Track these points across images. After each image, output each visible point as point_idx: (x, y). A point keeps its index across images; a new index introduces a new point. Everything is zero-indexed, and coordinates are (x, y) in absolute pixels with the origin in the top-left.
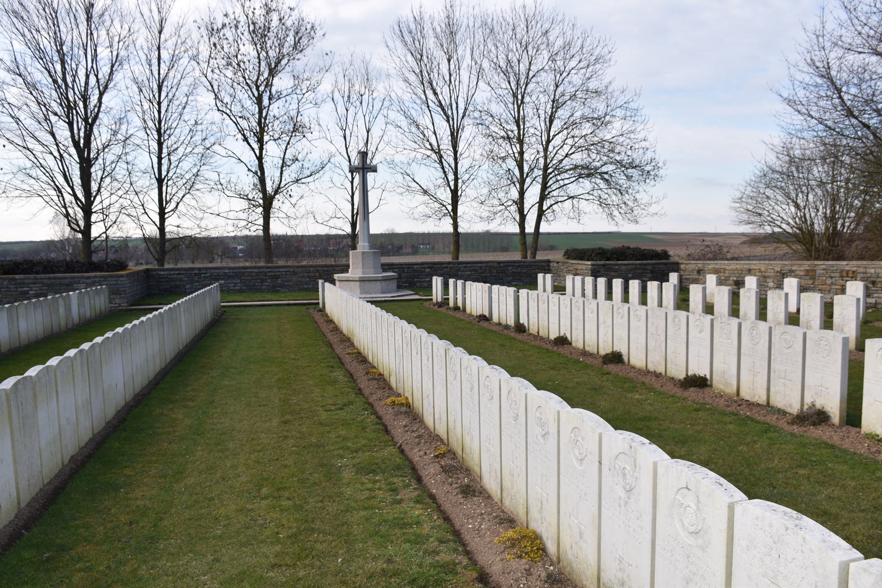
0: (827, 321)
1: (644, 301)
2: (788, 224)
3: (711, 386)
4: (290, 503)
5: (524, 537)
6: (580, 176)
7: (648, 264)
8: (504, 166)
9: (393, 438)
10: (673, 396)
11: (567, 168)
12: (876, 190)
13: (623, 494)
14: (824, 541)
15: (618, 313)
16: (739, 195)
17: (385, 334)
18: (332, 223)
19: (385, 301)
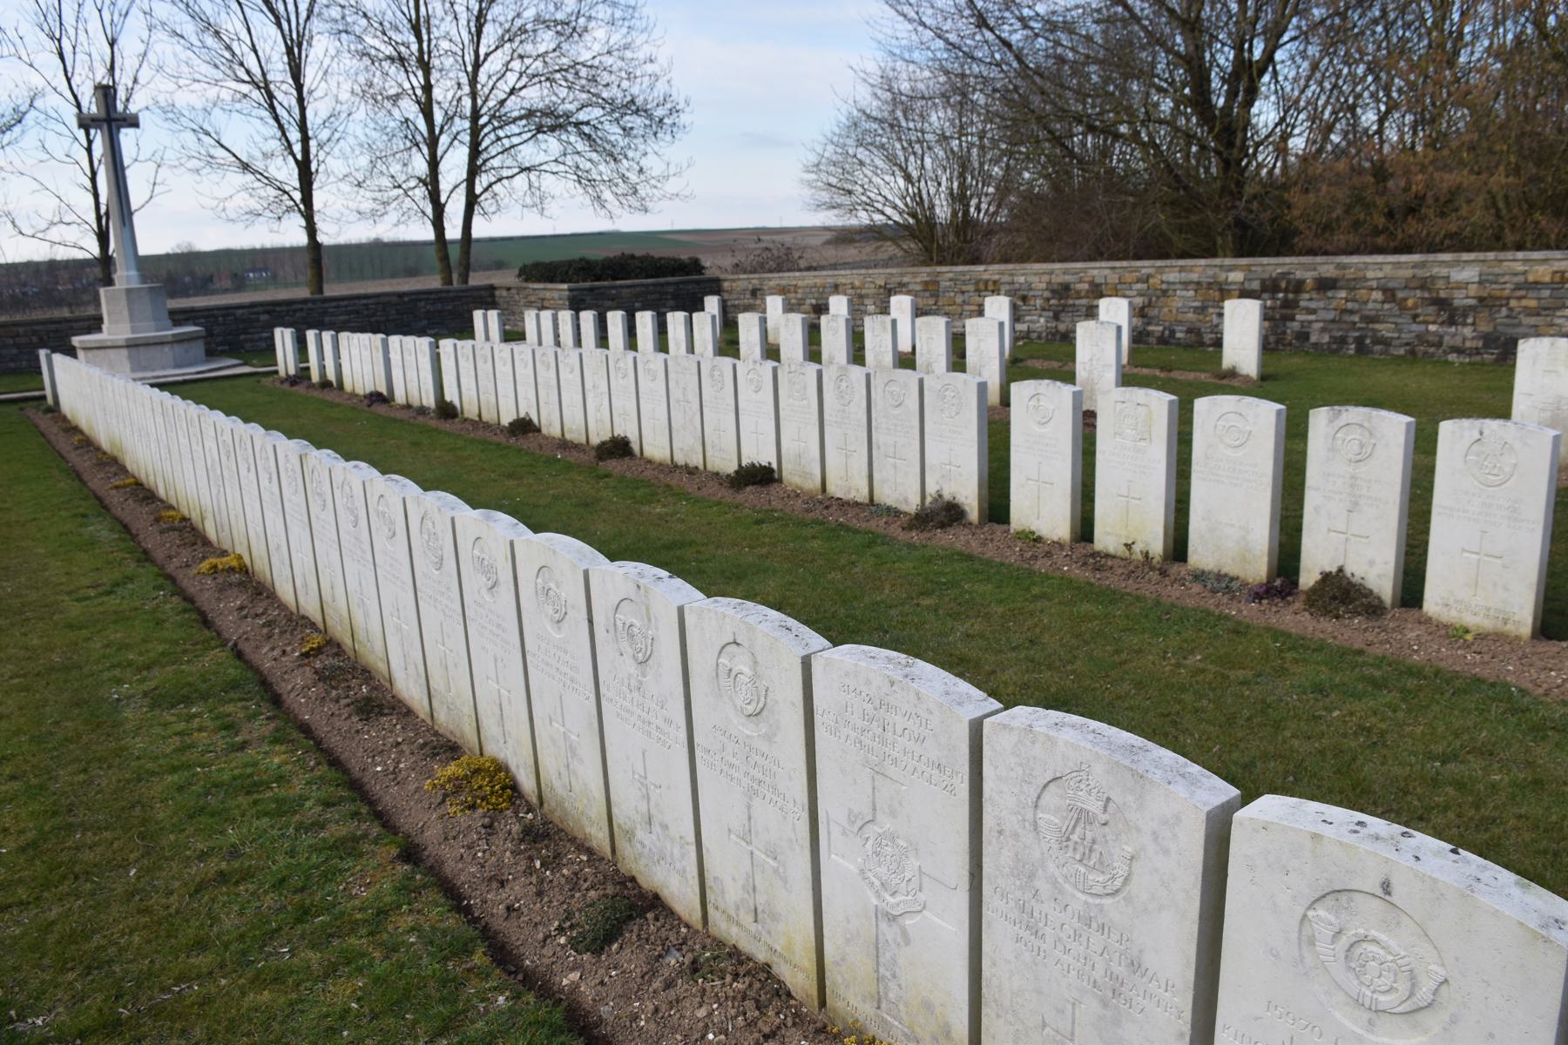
0: (958, 358)
1: (662, 345)
2: (895, 207)
3: (780, 480)
4: (16, 785)
5: (477, 771)
6: (539, 130)
7: (668, 284)
8: (396, 112)
9: (219, 634)
10: (719, 503)
11: (516, 114)
12: (1023, 149)
13: (632, 669)
14: (947, 693)
15: (617, 369)
16: (813, 159)
17: (184, 441)
18: (55, 234)
19: (185, 382)
